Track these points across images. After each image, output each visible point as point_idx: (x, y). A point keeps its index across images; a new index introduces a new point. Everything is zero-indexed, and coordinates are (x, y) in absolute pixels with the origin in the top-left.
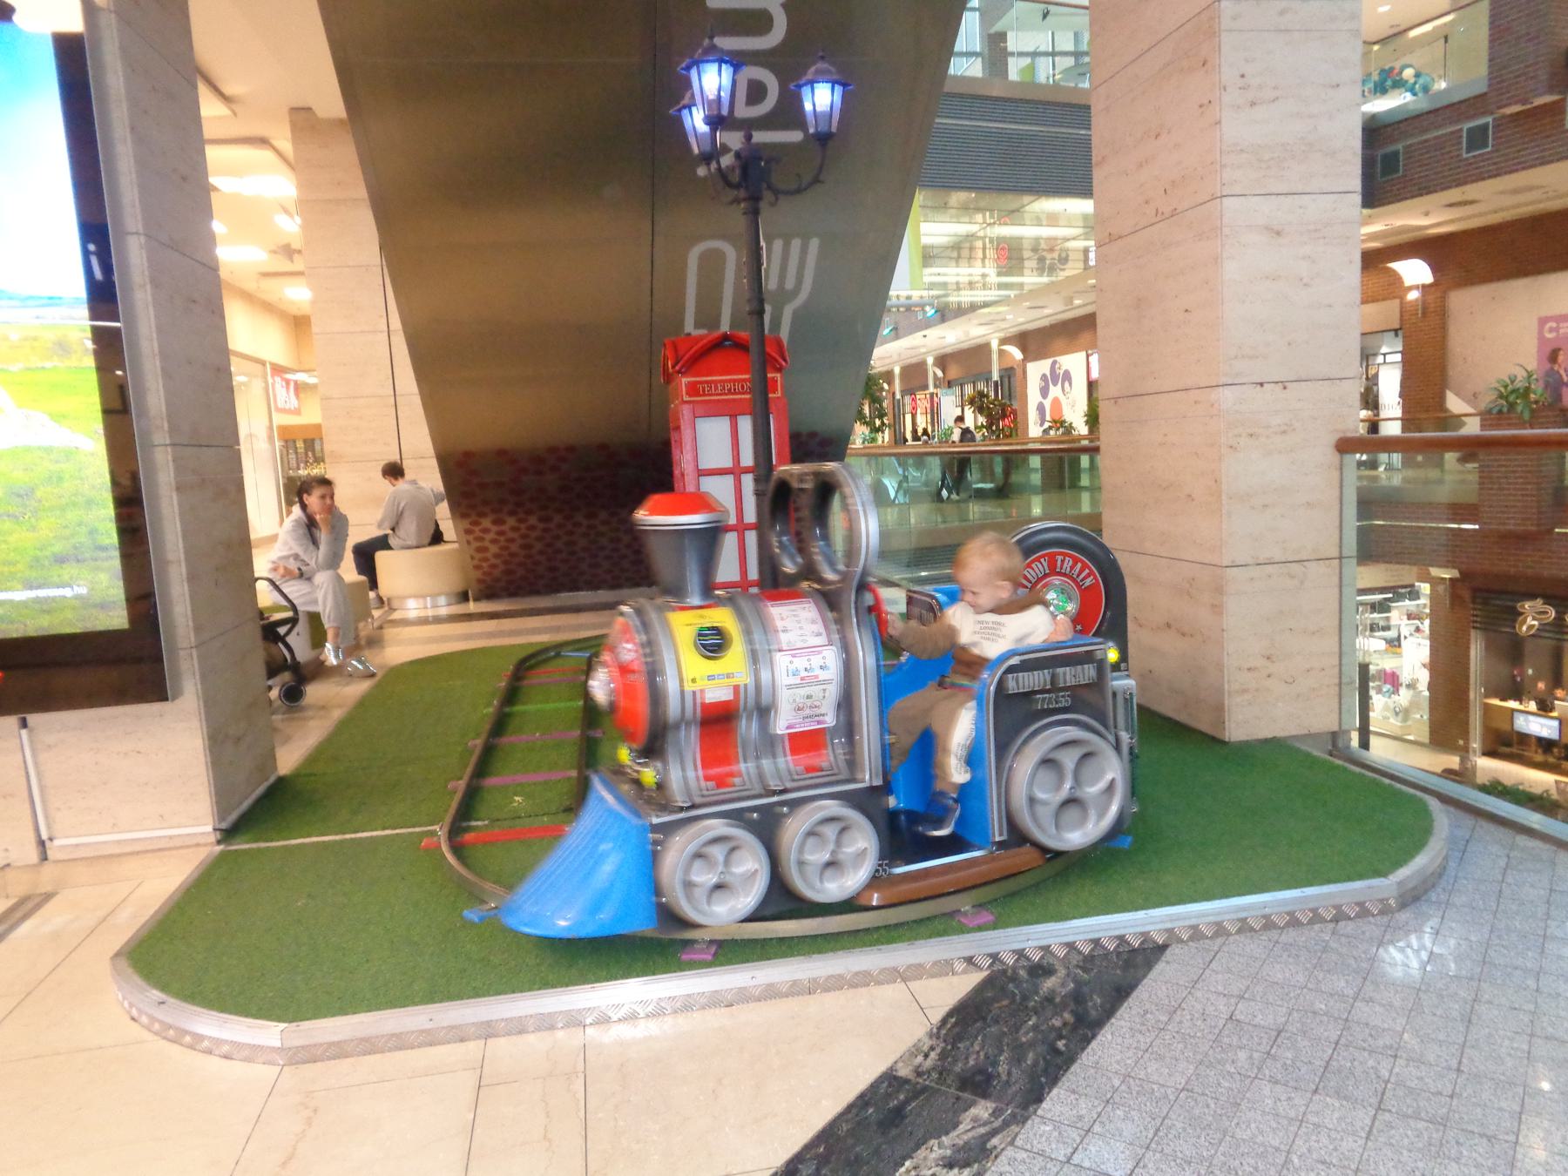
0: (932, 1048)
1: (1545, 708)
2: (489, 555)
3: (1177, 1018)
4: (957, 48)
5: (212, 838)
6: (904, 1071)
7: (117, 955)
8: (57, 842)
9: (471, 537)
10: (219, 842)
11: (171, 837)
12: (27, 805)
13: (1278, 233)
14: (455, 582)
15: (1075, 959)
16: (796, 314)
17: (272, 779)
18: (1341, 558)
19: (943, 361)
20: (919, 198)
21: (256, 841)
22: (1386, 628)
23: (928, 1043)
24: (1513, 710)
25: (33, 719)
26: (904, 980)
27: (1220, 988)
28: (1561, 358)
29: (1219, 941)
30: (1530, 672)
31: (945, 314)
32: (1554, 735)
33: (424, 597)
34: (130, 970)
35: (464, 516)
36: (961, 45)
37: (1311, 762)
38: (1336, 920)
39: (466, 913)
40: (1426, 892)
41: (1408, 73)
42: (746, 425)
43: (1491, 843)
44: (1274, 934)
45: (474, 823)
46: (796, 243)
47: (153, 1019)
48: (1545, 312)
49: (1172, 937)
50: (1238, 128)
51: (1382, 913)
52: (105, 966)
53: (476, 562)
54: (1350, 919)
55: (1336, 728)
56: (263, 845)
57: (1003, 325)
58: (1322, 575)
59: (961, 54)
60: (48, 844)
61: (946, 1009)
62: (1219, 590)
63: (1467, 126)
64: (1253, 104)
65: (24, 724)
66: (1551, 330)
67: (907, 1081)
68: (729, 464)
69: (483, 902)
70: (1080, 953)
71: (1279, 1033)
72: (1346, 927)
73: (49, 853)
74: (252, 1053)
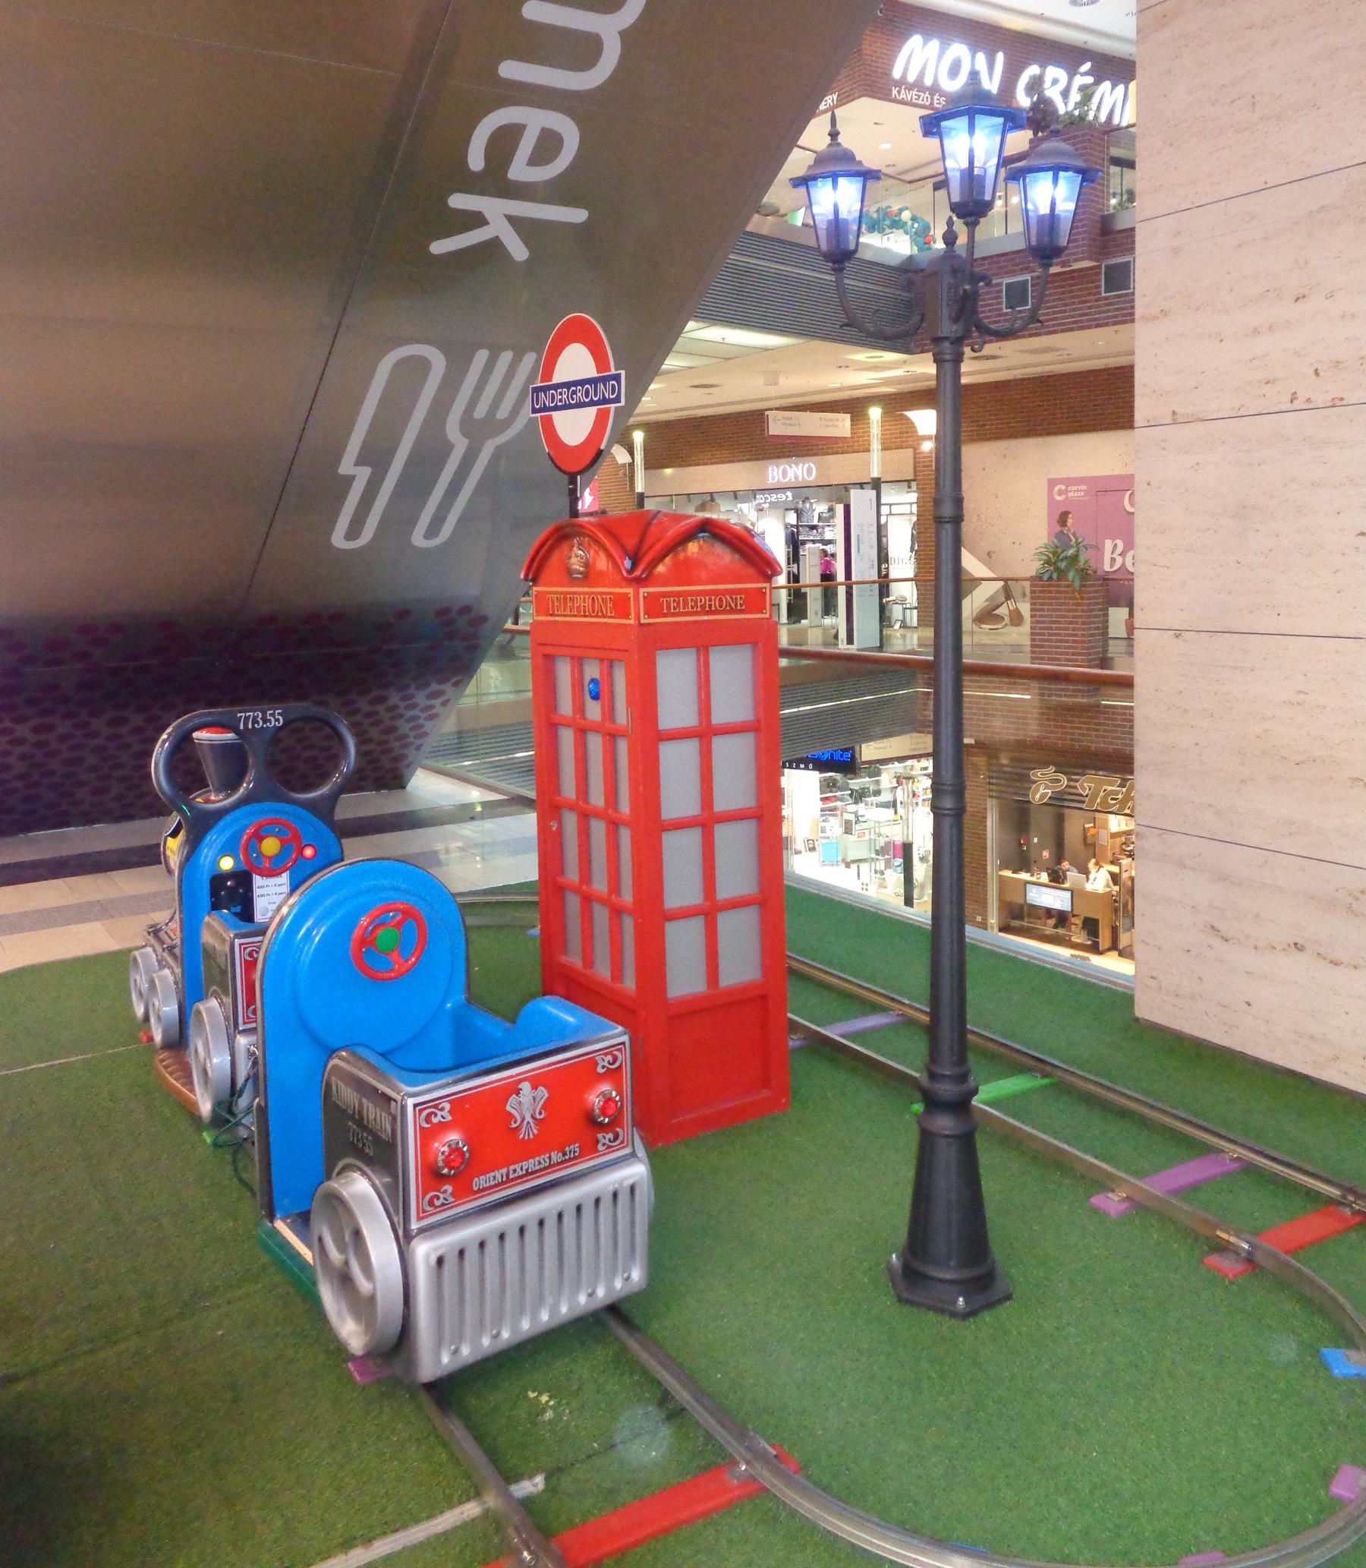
1: (1057, 879)
22: (877, 793)
24: (1027, 882)
28: (1070, 522)
30: (1036, 840)
32: (1067, 907)
41: (906, 215)
46: (507, 357)
48: (1056, 474)
63: (1006, 281)
66: (1060, 493)
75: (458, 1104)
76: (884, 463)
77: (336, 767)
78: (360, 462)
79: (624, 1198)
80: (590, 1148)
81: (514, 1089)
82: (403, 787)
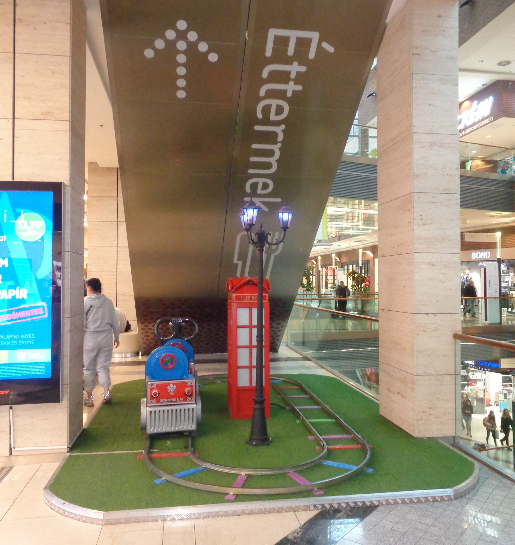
0: (300, 532)
2: (150, 338)
3: (375, 527)
4: (350, 134)
5: (66, 451)
6: (290, 537)
7: (45, 488)
8: (16, 449)
9: (143, 331)
10: (68, 452)
11: (53, 449)
12: (8, 436)
13: (433, 265)
14: (134, 348)
15: (348, 508)
16: (275, 257)
17: (82, 429)
18: (455, 375)
19: (339, 254)
20: (331, 199)
21: (81, 452)
23: (299, 530)
25: (14, 406)
26: (294, 511)
27: (391, 520)
29: (395, 506)
31: (340, 237)
33: (122, 353)
34: (51, 493)
35: (142, 323)
36: (352, 133)
37: (442, 447)
38: (433, 502)
39: (155, 481)
40: (465, 495)
42: (255, 311)
43: (494, 480)
44: (413, 505)
45: (154, 450)
47: (60, 508)
49: (380, 504)
50: (420, 231)
51: (449, 500)
52: (42, 491)
53: (144, 341)
54: (438, 501)
55: (454, 435)
56: (83, 454)
57: (365, 242)
58: (449, 380)
59: (352, 136)
60: (13, 449)
61: (306, 521)
62: (413, 383)
64: (424, 224)
65: (11, 408)
67: (291, 540)
68: (248, 344)
69: (161, 478)
70: (350, 506)
71: (405, 534)
72: (436, 504)
73: (13, 453)
74: (93, 521)
75: (157, 385)
76: (502, 254)
77: (193, 333)
78: (239, 260)
79: (191, 410)
80: (185, 399)
81: (169, 384)
82: (277, 352)
